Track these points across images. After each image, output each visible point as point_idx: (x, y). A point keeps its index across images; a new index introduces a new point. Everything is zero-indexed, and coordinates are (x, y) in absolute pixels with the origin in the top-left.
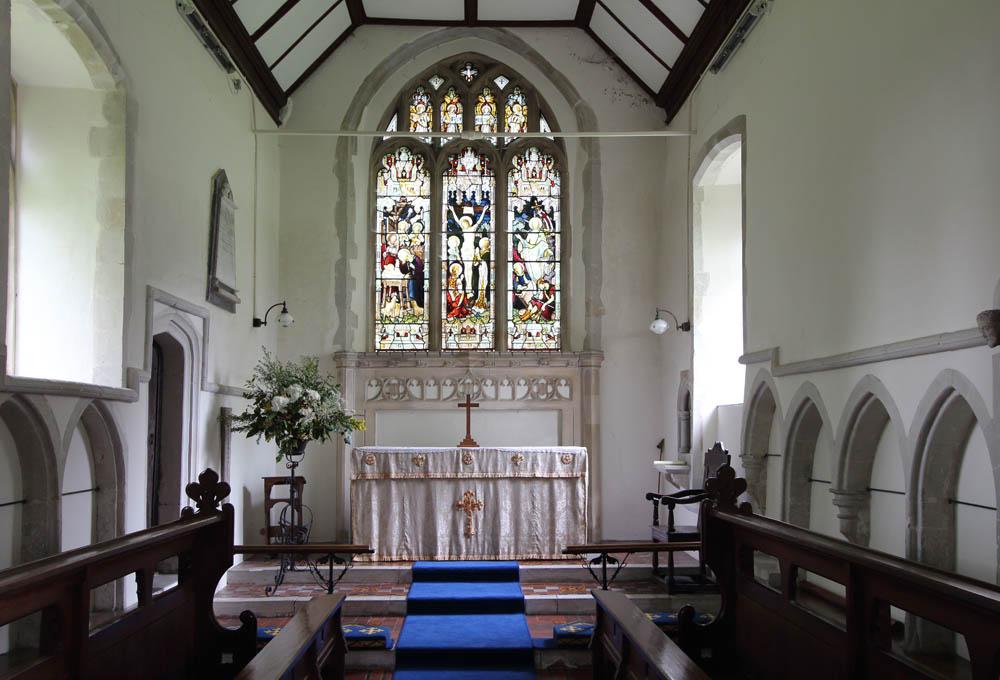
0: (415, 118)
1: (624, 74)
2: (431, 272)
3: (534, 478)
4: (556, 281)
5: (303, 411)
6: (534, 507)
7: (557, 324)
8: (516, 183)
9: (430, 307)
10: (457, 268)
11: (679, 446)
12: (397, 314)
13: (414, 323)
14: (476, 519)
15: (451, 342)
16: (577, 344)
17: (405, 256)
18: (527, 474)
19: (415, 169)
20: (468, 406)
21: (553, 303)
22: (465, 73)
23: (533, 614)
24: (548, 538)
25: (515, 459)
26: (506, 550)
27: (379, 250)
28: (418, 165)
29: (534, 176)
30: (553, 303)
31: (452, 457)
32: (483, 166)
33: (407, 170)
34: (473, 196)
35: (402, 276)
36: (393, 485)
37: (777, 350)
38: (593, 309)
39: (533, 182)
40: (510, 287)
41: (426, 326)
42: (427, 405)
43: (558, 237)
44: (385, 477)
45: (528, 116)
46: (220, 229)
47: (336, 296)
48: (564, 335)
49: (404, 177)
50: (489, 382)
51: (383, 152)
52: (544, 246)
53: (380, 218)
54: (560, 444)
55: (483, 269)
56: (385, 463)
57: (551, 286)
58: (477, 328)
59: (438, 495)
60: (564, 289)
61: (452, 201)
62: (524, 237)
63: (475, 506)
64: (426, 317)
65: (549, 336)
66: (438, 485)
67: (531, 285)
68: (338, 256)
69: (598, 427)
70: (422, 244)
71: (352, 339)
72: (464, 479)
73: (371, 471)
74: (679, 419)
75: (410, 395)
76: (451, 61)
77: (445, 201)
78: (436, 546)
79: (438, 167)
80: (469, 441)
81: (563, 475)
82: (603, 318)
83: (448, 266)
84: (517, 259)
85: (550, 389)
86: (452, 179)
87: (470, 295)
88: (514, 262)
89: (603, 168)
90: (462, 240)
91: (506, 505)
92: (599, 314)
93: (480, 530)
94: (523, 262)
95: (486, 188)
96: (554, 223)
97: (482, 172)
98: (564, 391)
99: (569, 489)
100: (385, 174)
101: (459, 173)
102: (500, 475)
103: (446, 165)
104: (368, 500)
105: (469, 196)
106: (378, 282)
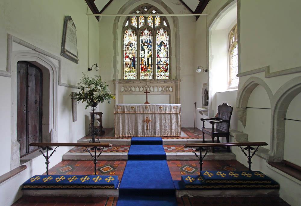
0: (133, 21)
1: (185, 8)
2: (137, 60)
3: (166, 113)
4: (168, 62)
5: (94, 93)
6: (166, 122)
7: (168, 73)
8: (158, 37)
9: (137, 69)
10: (144, 59)
11: (203, 104)
12: (129, 70)
13: (133, 73)
14: (149, 125)
15: (142, 78)
16: (173, 77)
17: (131, 56)
18: (164, 112)
19: (133, 34)
20: (147, 92)
21: (167, 68)
22: (145, 9)
23: (169, 160)
24: (170, 130)
25: (160, 108)
26: (158, 134)
27: (124, 54)
28: (134, 33)
29: (162, 36)
30: (167, 68)
31: (142, 107)
32: (150, 33)
33: (131, 34)
34: (147, 41)
35: (130, 61)
36: (126, 115)
37: (268, 67)
38: (178, 68)
39: (162, 37)
40: (157, 64)
41: (136, 74)
42: (137, 93)
43: (168, 51)
44: (123, 113)
45: (161, 20)
46: (67, 33)
47: (114, 65)
48: (170, 76)
49: (130, 36)
50: (152, 87)
51: (125, 29)
52: (165, 53)
53: (125, 46)
54: (170, 103)
55: (150, 59)
56: (123, 109)
57: (167, 63)
58: (149, 74)
59: (139, 118)
60: (170, 64)
61: (142, 42)
62: (160, 51)
63: (149, 121)
64: (136, 71)
65: (166, 76)
66: (139, 115)
67: (162, 63)
68: (114, 55)
69: (180, 99)
70: (135, 53)
71: (118, 77)
72: (146, 113)
73: (119, 111)
74: (202, 97)
75: (132, 91)
76: (141, 6)
77: (140, 42)
78: (138, 133)
79: (139, 33)
80: (147, 103)
81: (174, 112)
82: (180, 71)
83: (141, 58)
84: (158, 56)
85: (167, 89)
86: (142, 37)
87: (147, 66)
88: (158, 57)
89: (180, 32)
90: (145, 52)
91: (158, 121)
92: (179, 70)
93: (151, 128)
94: (160, 57)
95: (150, 39)
96: (167, 48)
97: (150, 35)
98: (171, 89)
99: (176, 116)
100: (126, 35)
101: (144, 35)
102: (156, 112)
103: (141, 33)
104: (119, 118)
105: (146, 41)
106: (124, 63)
